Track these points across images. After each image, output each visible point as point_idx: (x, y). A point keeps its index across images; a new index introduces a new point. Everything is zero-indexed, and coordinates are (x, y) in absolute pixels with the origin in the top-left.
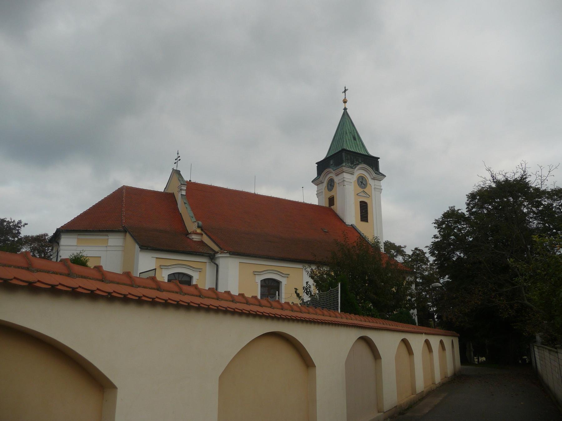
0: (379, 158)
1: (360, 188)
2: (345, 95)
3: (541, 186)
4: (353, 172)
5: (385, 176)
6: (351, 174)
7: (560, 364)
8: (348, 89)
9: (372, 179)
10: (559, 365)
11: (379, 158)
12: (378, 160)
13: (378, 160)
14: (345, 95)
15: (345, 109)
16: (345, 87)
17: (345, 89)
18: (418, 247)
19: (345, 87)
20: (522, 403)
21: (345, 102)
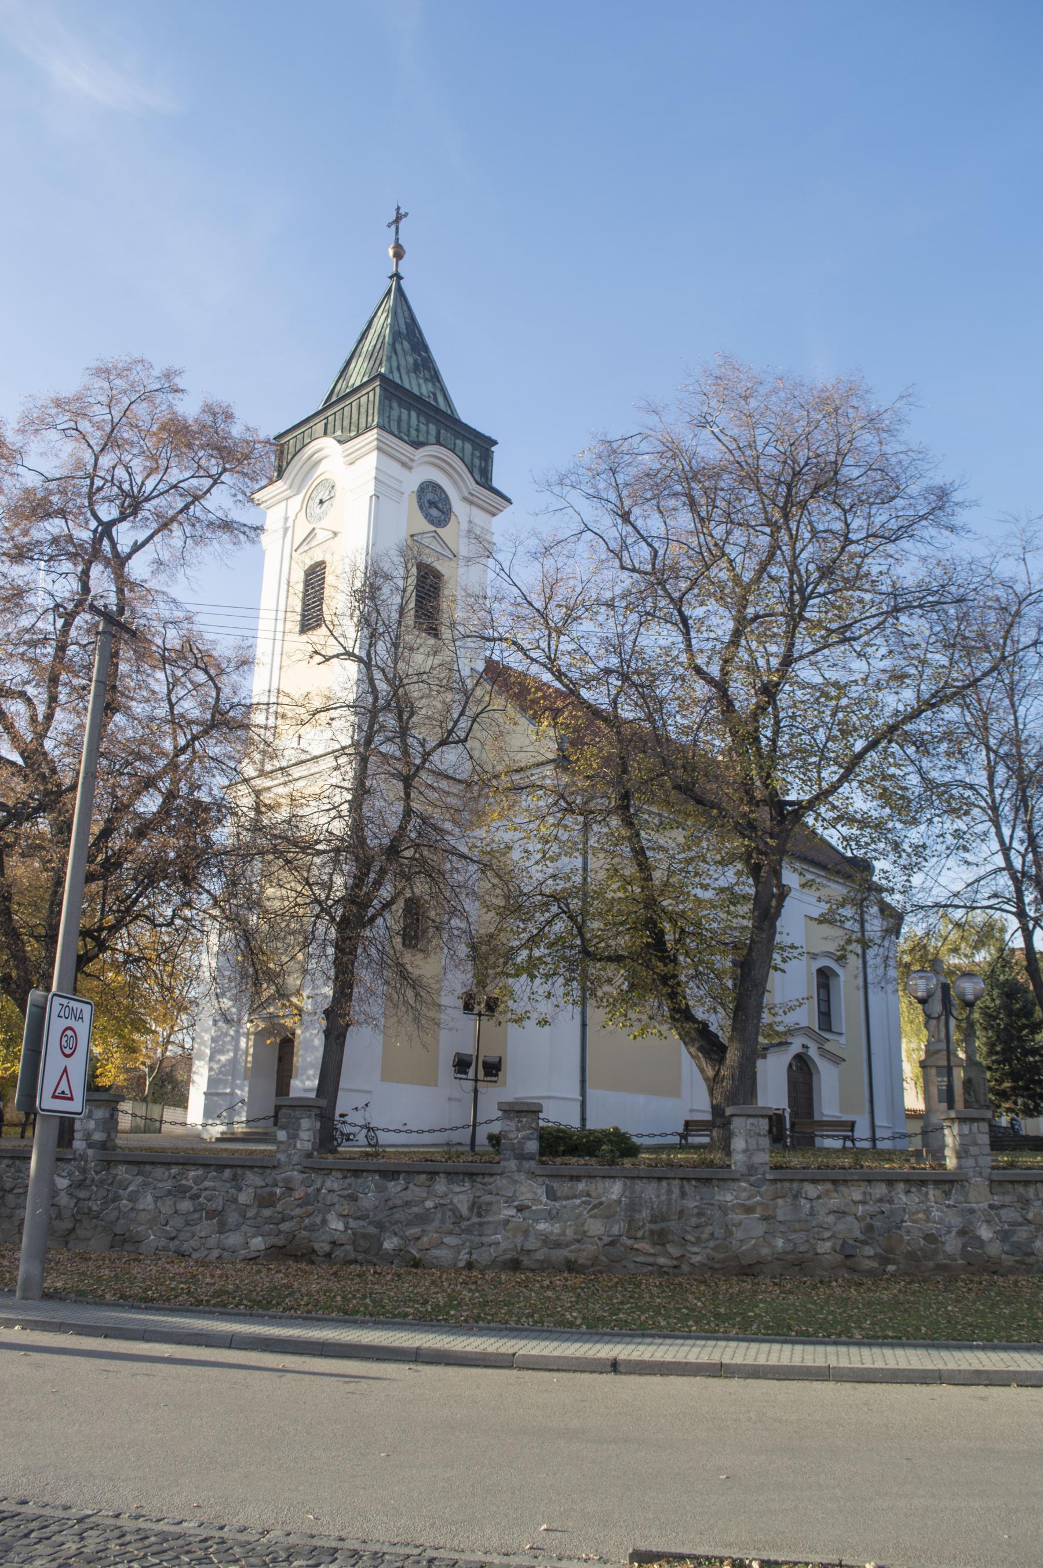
0: (495, 443)
1: (405, 248)
2: (397, 233)
3: (639, 853)
4: (412, 460)
5: (509, 501)
6: (404, 464)
7: (290, 501)
8: (406, 215)
9: (465, 499)
10: (287, 499)
11: (495, 443)
12: (493, 449)
13: (493, 449)
14: (397, 233)
15: (397, 276)
16: (398, 208)
17: (398, 213)
18: (136, 541)
19: (398, 208)
20: (752, 1314)
21: (399, 254)
